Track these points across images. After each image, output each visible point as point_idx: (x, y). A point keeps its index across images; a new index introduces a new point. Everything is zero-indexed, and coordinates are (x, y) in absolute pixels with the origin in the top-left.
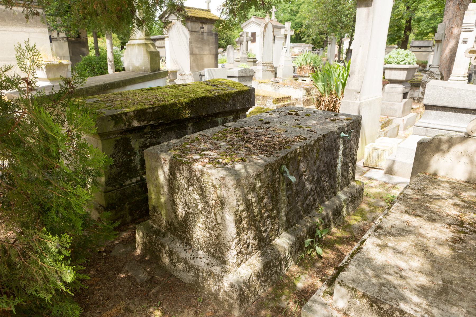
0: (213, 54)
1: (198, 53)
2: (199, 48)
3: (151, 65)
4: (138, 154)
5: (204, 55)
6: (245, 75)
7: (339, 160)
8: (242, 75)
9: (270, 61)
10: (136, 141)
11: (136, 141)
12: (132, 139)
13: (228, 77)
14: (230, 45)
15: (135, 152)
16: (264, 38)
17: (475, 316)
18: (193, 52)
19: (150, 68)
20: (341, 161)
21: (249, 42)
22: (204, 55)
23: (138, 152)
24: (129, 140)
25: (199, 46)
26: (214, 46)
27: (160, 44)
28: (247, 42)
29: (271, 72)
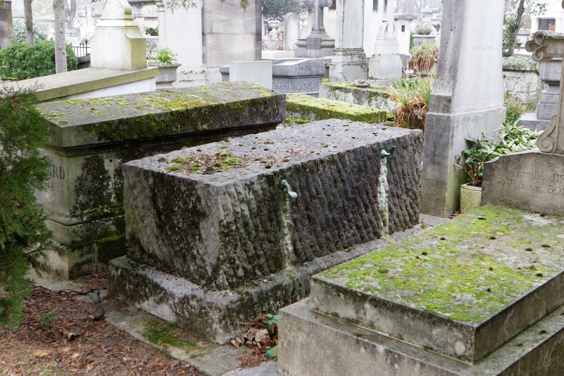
0: (252, 33)
1: (221, 30)
2: (223, 21)
3: (132, 58)
4: (113, 180)
5: (234, 34)
6: (308, 73)
7: (382, 187)
8: (300, 74)
9: (358, 47)
10: (111, 161)
11: (111, 161)
12: (106, 158)
13: (561, 61)
14: (290, 13)
15: (109, 176)
16: (344, 4)
17: (30, 2)
18: (212, 30)
19: (131, 64)
20: (386, 190)
21: (326, 9)
22: (234, 34)
23: (112, 176)
24: (101, 162)
25: (223, 18)
26: (254, 18)
27: (149, 12)
28: (322, 8)
29: (359, 67)
